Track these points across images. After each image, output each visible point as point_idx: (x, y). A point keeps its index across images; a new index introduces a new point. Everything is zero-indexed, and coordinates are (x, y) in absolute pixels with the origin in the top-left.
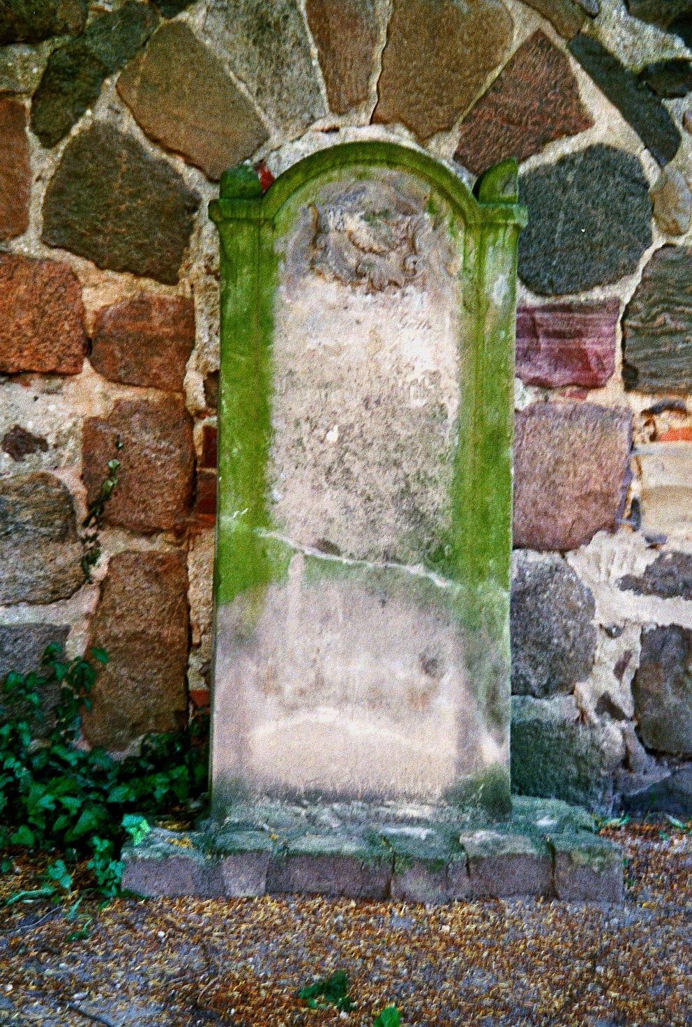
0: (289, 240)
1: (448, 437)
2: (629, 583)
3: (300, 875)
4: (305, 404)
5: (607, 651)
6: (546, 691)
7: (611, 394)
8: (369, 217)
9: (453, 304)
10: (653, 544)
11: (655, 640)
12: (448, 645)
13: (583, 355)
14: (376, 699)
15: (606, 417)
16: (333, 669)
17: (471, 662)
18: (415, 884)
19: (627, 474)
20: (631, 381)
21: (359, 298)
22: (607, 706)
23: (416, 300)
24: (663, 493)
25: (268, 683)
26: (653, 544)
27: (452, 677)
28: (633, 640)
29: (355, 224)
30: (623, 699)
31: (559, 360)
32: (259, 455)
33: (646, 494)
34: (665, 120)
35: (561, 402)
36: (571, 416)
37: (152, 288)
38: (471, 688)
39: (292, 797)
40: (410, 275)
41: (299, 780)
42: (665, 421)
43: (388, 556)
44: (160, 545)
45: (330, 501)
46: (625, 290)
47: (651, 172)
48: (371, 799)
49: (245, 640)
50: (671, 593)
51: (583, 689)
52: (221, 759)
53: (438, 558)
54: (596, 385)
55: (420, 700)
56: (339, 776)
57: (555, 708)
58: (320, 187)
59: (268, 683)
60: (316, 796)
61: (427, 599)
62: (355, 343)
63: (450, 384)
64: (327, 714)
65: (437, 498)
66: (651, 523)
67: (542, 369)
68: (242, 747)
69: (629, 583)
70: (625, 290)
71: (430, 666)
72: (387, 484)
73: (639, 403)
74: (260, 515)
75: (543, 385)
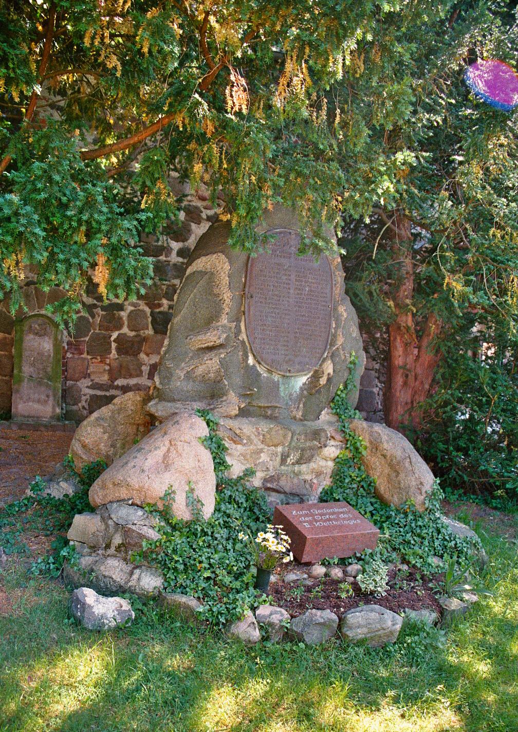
0: (26, 328)
1: (51, 359)
2: (87, 387)
3: (24, 427)
4: (253, 437)
5: (84, 398)
6: (74, 405)
7: (85, 356)
8: (39, 325)
9: (52, 339)
10: (92, 381)
11: (92, 397)
12: (51, 393)
13: (79, 349)
14: (39, 401)
15: (84, 359)
16: (32, 396)
17: (54, 396)
18: (43, 429)
19: (87, 369)
20: (88, 354)
21: (37, 337)
22: (84, 408)
23: (47, 338)
24: (94, 372)
25: (21, 398)
26: (92, 381)
27: (51, 398)
28: (88, 397)
29: (36, 326)
30: (87, 407)
31: (76, 349)
32: (20, 361)
33: (91, 372)
34: (93, 312)
35: (76, 356)
36: (78, 359)
37: (7, 335)
38: (54, 400)
39: (24, 417)
40: (45, 334)
41: (26, 414)
42: (94, 360)
43: (41, 378)
44: (7, 378)
45: (32, 369)
46: (87, 339)
47: (91, 320)
48: (38, 417)
49: (17, 391)
50: (94, 389)
51: (80, 404)
52: (13, 410)
53: (49, 379)
54: (82, 354)
55: (46, 402)
56: (33, 413)
57: (75, 408)
58: (31, 320)
59: (21, 398)
60: (28, 417)
61: (47, 386)
62: (36, 344)
63: (51, 351)
64: (31, 404)
65: (49, 369)
66: (92, 377)
67: (73, 351)
68: (17, 408)
69: (87, 387)
70: (87, 339)
71: (48, 396)
72: (41, 367)
73: (89, 357)
74: (20, 371)
75: (73, 354)
